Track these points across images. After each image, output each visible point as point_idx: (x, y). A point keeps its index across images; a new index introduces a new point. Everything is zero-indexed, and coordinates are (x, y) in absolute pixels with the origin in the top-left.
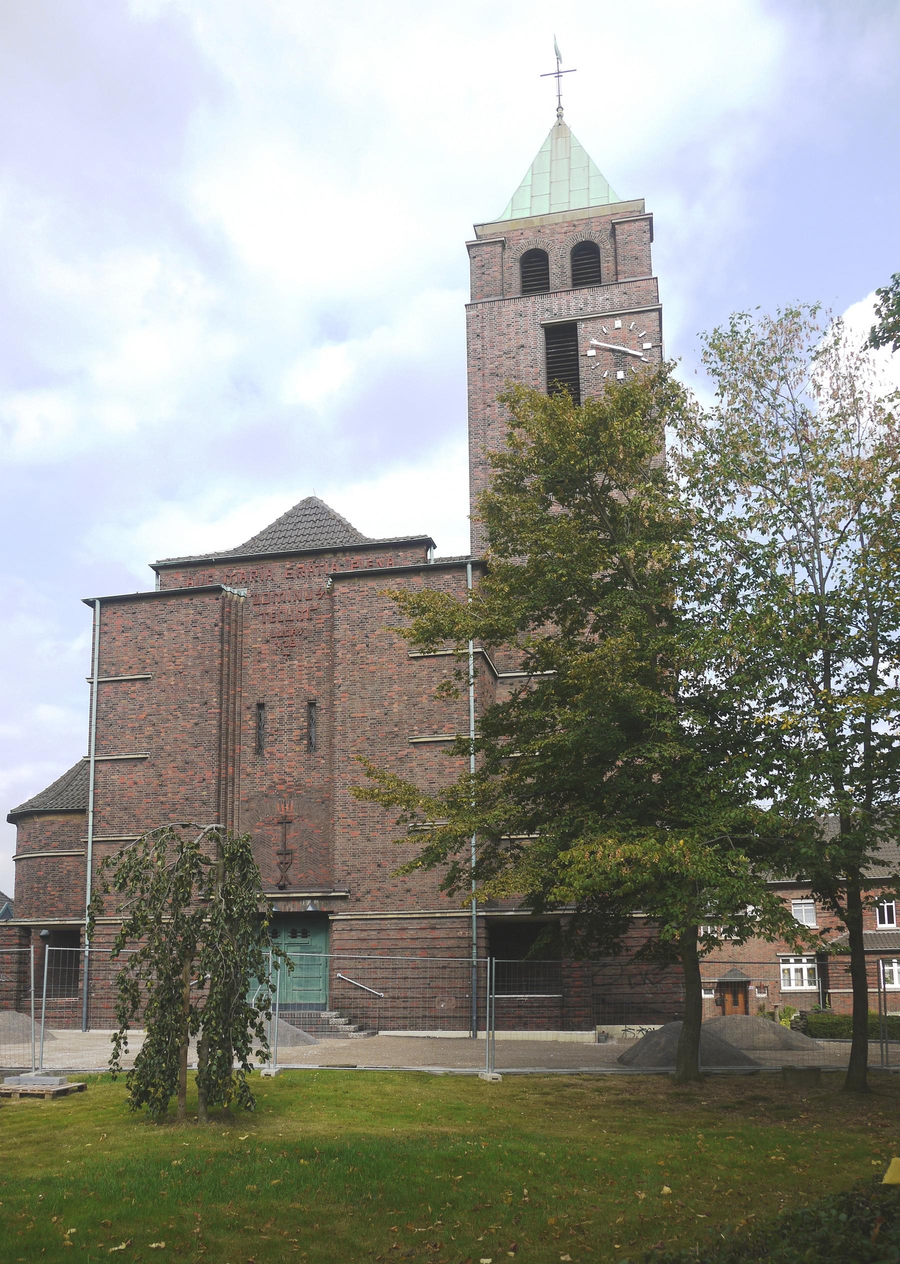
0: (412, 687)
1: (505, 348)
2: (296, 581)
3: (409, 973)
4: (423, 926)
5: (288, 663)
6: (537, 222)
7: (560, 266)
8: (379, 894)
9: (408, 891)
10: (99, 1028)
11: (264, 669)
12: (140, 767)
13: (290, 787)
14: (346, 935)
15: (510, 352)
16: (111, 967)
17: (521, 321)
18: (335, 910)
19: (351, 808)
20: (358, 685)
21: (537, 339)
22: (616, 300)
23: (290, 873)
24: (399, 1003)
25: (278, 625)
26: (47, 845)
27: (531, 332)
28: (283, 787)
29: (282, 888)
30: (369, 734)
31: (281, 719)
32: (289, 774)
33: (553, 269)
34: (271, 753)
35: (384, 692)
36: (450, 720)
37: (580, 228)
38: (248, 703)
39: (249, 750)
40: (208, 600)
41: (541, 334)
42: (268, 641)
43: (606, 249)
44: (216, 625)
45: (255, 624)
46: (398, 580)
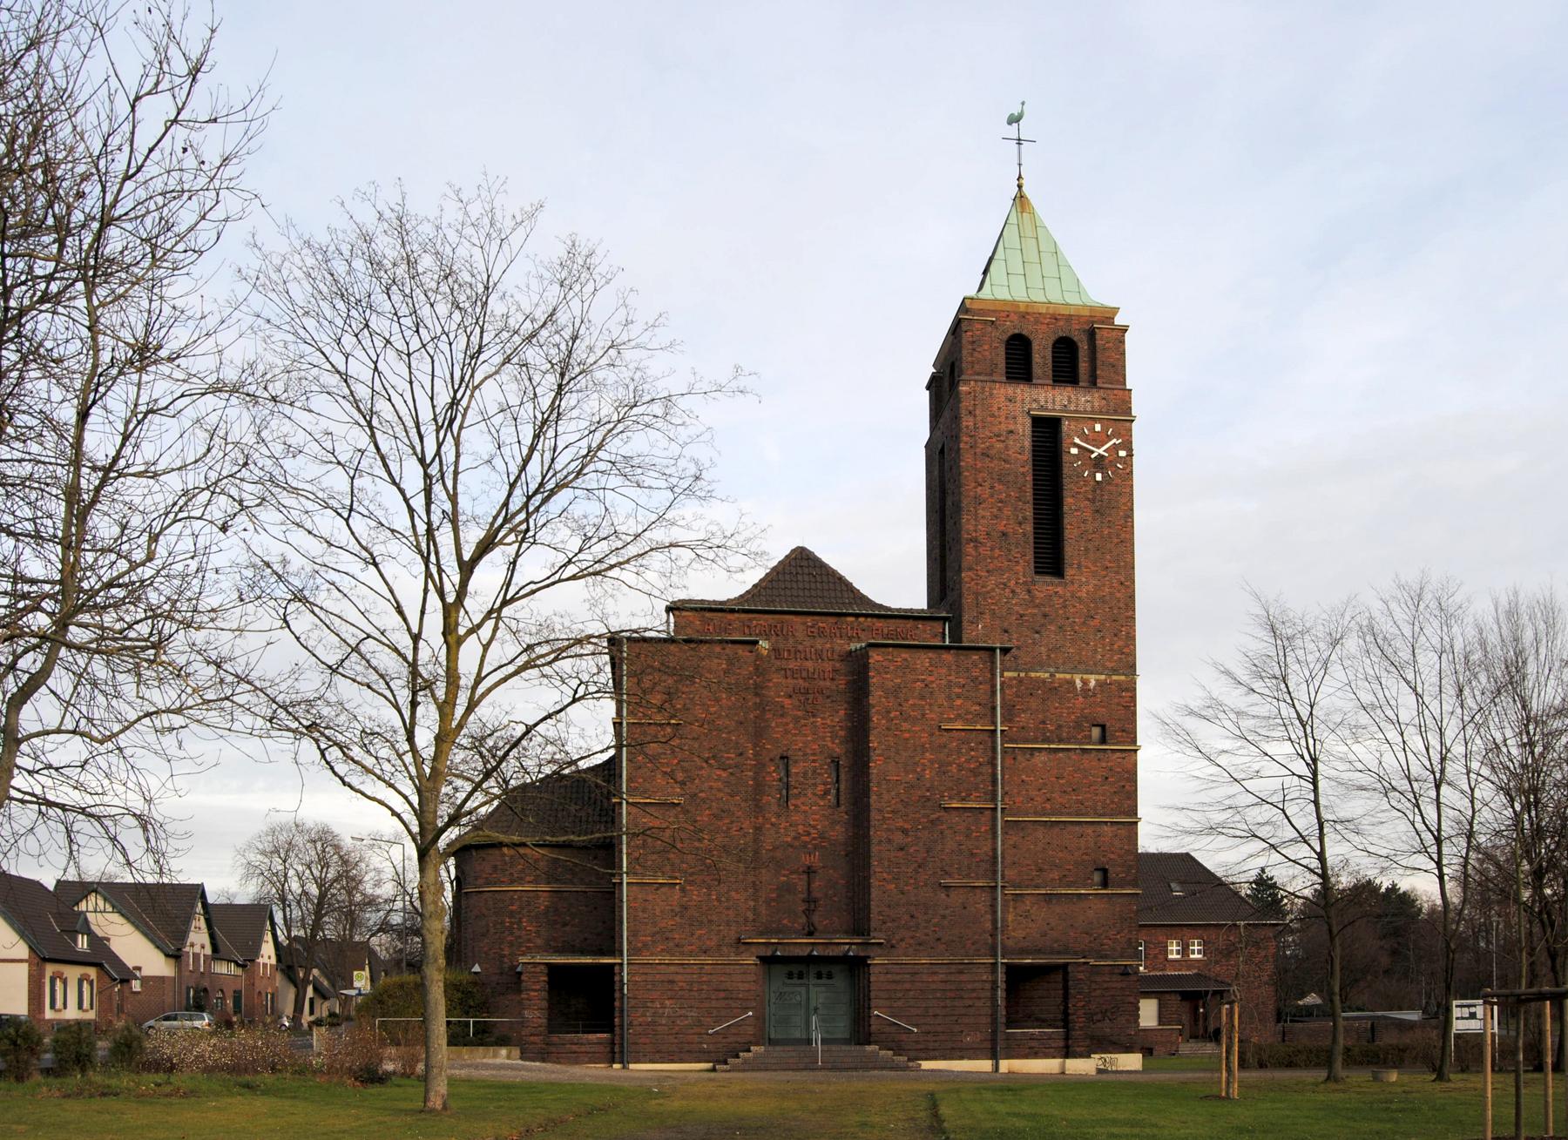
1: (996, 430)
6: (1022, 309)
7: (1042, 357)
12: (673, 812)
14: (882, 978)
21: (1024, 427)
23: (816, 918)
24: (930, 1037)
27: (1020, 420)
28: (807, 839)
29: (810, 934)
31: (805, 773)
32: (814, 827)
33: (1036, 358)
36: (976, 789)
40: (741, 651)
41: (1028, 422)
43: (1083, 347)
45: (777, 678)
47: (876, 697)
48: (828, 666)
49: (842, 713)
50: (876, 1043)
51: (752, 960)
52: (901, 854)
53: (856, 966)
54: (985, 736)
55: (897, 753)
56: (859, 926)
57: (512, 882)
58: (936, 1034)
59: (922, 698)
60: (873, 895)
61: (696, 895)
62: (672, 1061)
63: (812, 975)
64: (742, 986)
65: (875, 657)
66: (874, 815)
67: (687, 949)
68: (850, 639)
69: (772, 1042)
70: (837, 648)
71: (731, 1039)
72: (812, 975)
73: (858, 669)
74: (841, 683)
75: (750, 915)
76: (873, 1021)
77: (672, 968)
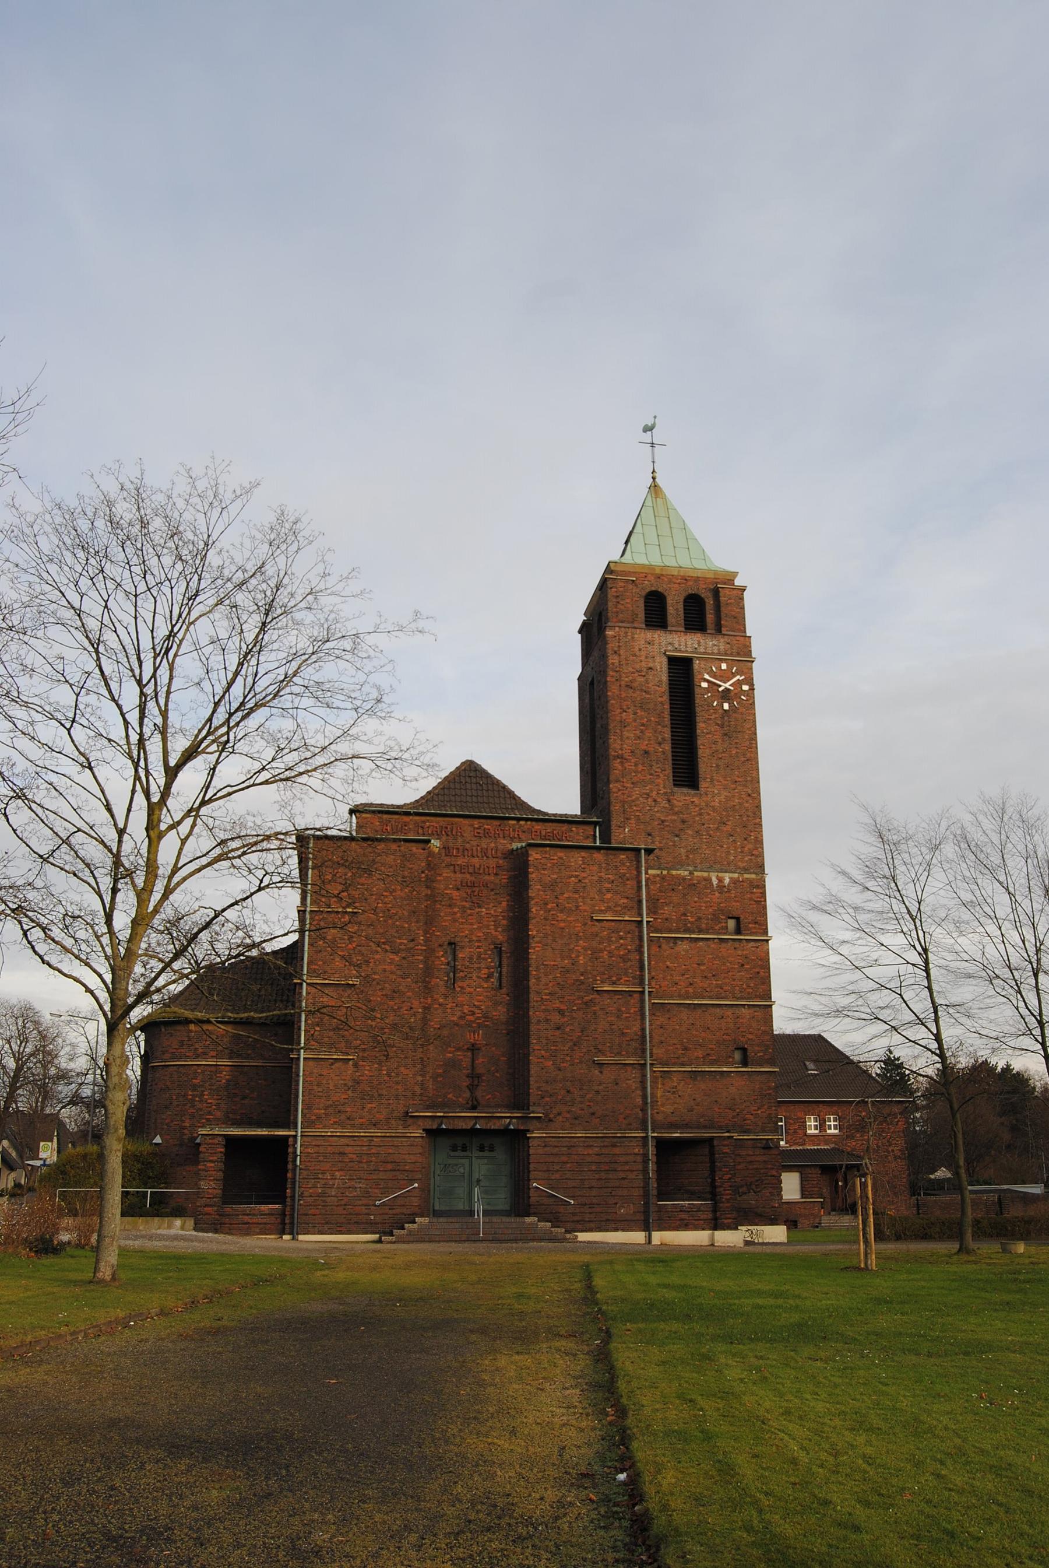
0: (594, 944)
1: (638, 667)
2: (484, 840)
3: (594, 1184)
4: (606, 1144)
5: (477, 910)
6: (658, 571)
7: (675, 609)
8: (568, 1116)
9: (593, 1114)
10: (308, 1234)
11: (455, 913)
13: (478, 1018)
14: (541, 1151)
15: (640, 671)
16: (320, 1176)
17: (650, 647)
18: (531, 1128)
19: (544, 1042)
20: (550, 937)
22: (722, 647)
23: (479, 1093)
25: (468, 876)
26: (204, 1053)
27: (658, 659)
29: (474, 1108)
30: (559, 980)
31: (471, 958)
32: (478, 1007)
33: (671, 610)
34: (462, 988)
35: (572, 946)
37: (691, 583)
38: (440, 942)
39: (441, 983)
41: (665, 661)
42: (458, 889)
43: (710, 602)
44: (423, 872)
45: (447, 873)
46: (583, 854)
47: (535, 891)
48: (492, 863)
49: (504, 904)
50: (534, 1214)
52: (558, 1033)
54: (633, 926)
55: (554, 940)
56: (520, 1101)
57: (197, 1057)
59: (576, 892)
62: (340, 1233)
65: (534, 855)
66: (533, 997)
67: (358, 1122)
68: (512, 839)
69: (437, 1214)
70: (500, 847)
71: (398, 1210)
73: (518, 865)
74: (504, 878)
75: (418, 1089)
76: (532, 1193)
77: (343, 1141)
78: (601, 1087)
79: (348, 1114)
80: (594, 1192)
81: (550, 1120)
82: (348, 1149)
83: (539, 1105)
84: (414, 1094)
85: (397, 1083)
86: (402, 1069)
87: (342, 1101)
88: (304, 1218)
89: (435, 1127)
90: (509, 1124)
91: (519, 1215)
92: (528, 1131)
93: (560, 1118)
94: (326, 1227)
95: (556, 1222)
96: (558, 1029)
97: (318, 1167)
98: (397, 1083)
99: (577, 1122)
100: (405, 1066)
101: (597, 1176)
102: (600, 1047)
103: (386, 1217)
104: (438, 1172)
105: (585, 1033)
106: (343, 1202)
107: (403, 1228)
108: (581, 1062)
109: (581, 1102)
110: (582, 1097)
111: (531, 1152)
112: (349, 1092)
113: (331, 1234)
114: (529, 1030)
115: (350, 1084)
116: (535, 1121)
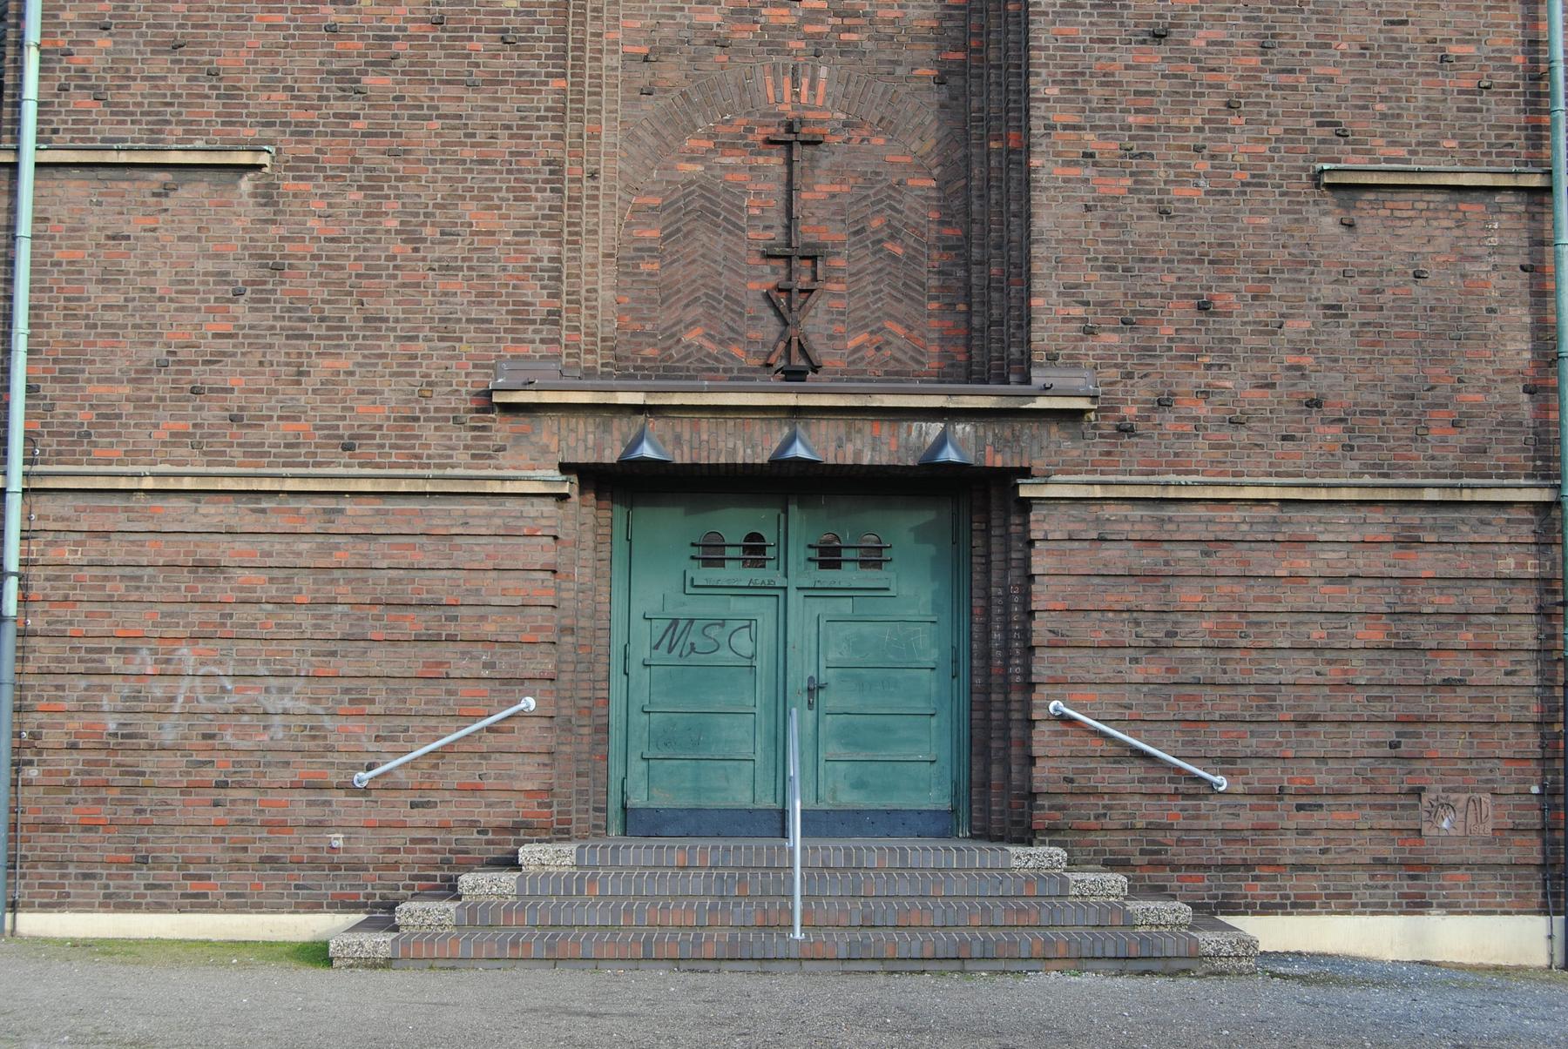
4: (1371, 533)
8: (1203, 410)
9: (1315, 403)
14: (1082, 558)
16: (112, 662)
18: (1038, 464)
23: (816, 323)
29: (793, 375)
50: (1053, 833)
51: (547, 477)
52: (1155, 56)
53: (974, 505)
56: (988, 333)
58: (1309, 798)
60: (1043, 221)
61: (317, 213)
62: (197, 902)
63: (798, 553)
64: (497, 589)
67: (275, 433)
69: (637, 823)
71: (447, 812)
72: (798, 553)
75: (536, 295)
76: (1043, 739)
77: (213, 513)
78: (1348, 291)
79: (234, 401)
80: (1321, 741)
81: (1125, 430)
82: (224, 550)
83: (1074, 362)
84: (520, 315)
85: (447, 269)
86: (469, 210)
87: (210, 345)
88: (43, 839)
89: (611, 456)
90: (941, 442)
91: (984, 834)
92: (1026, 472)
93: (1168, 420)
94: (139, 879)
95: (1150, 868)
96: (1159, 37)
97: (104, 626)
98: (447, 269)
99: (1243, 435)
100: (484, 197)
101: (1333, 674)
102: (1343, 115)
103: (399, 838)
104: (641, 651)
105: (1278, 57)
106: (212, 775)
107: (450, 890)
108: (1258, 181)
109: (1260, 354)
110: (1270, 330)
111: (1039, 564)
112: (240, 309)
113: (160, 907)
114: (1025, 46)
115: (242, 273)
116: (1055, 432)
